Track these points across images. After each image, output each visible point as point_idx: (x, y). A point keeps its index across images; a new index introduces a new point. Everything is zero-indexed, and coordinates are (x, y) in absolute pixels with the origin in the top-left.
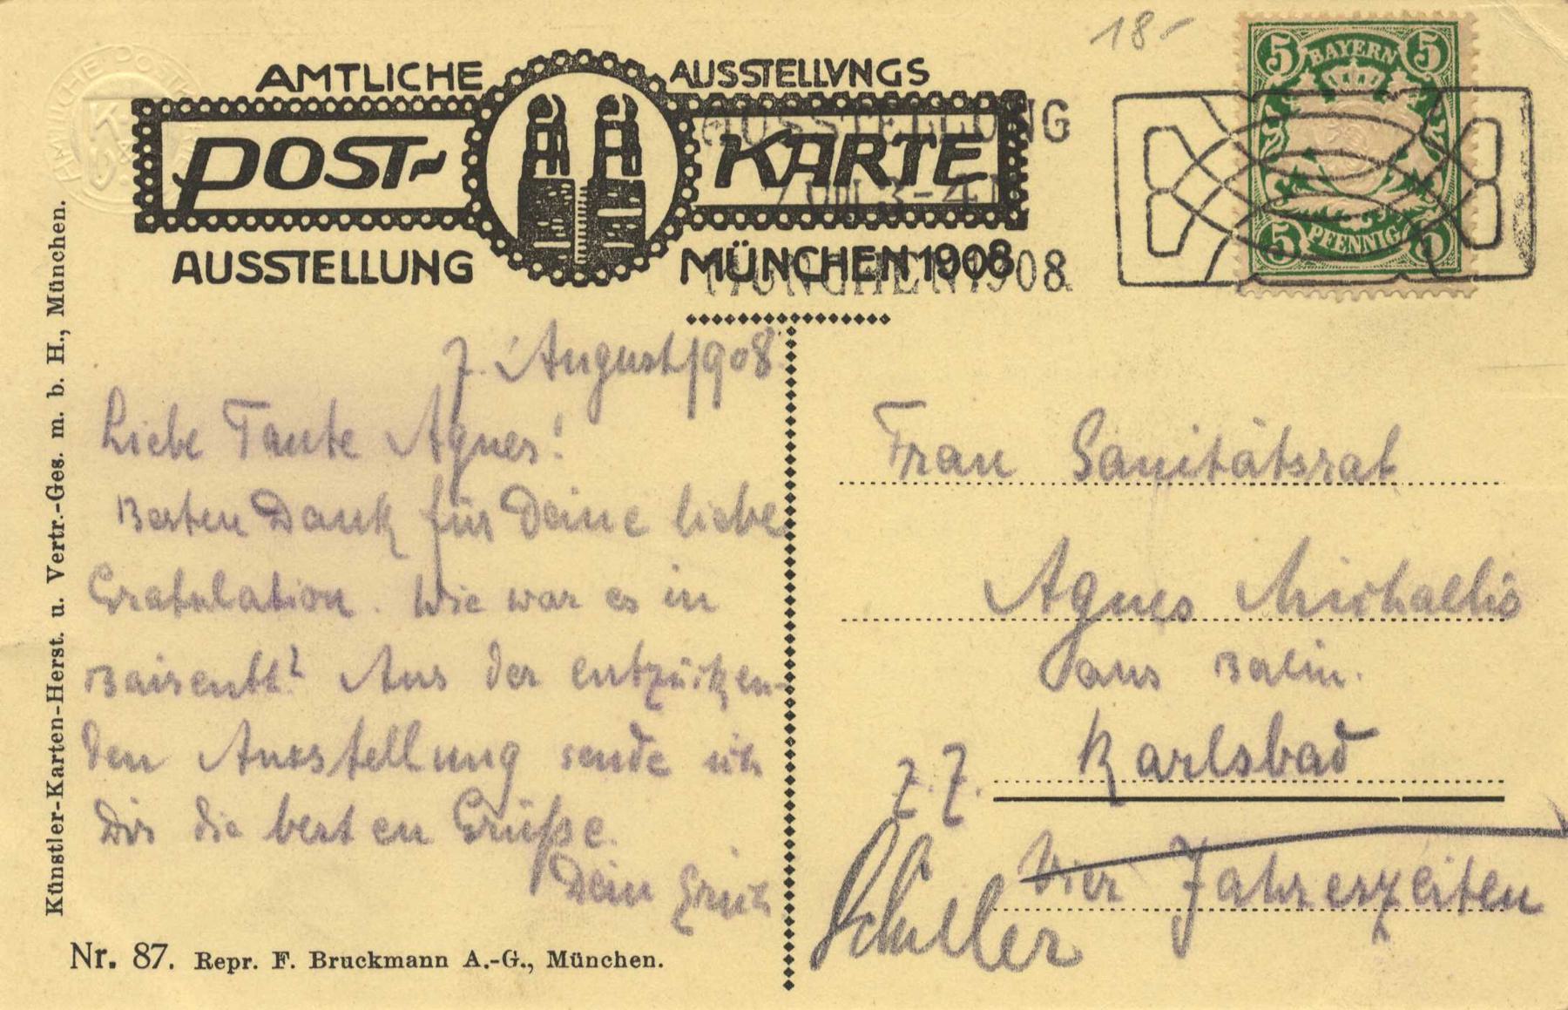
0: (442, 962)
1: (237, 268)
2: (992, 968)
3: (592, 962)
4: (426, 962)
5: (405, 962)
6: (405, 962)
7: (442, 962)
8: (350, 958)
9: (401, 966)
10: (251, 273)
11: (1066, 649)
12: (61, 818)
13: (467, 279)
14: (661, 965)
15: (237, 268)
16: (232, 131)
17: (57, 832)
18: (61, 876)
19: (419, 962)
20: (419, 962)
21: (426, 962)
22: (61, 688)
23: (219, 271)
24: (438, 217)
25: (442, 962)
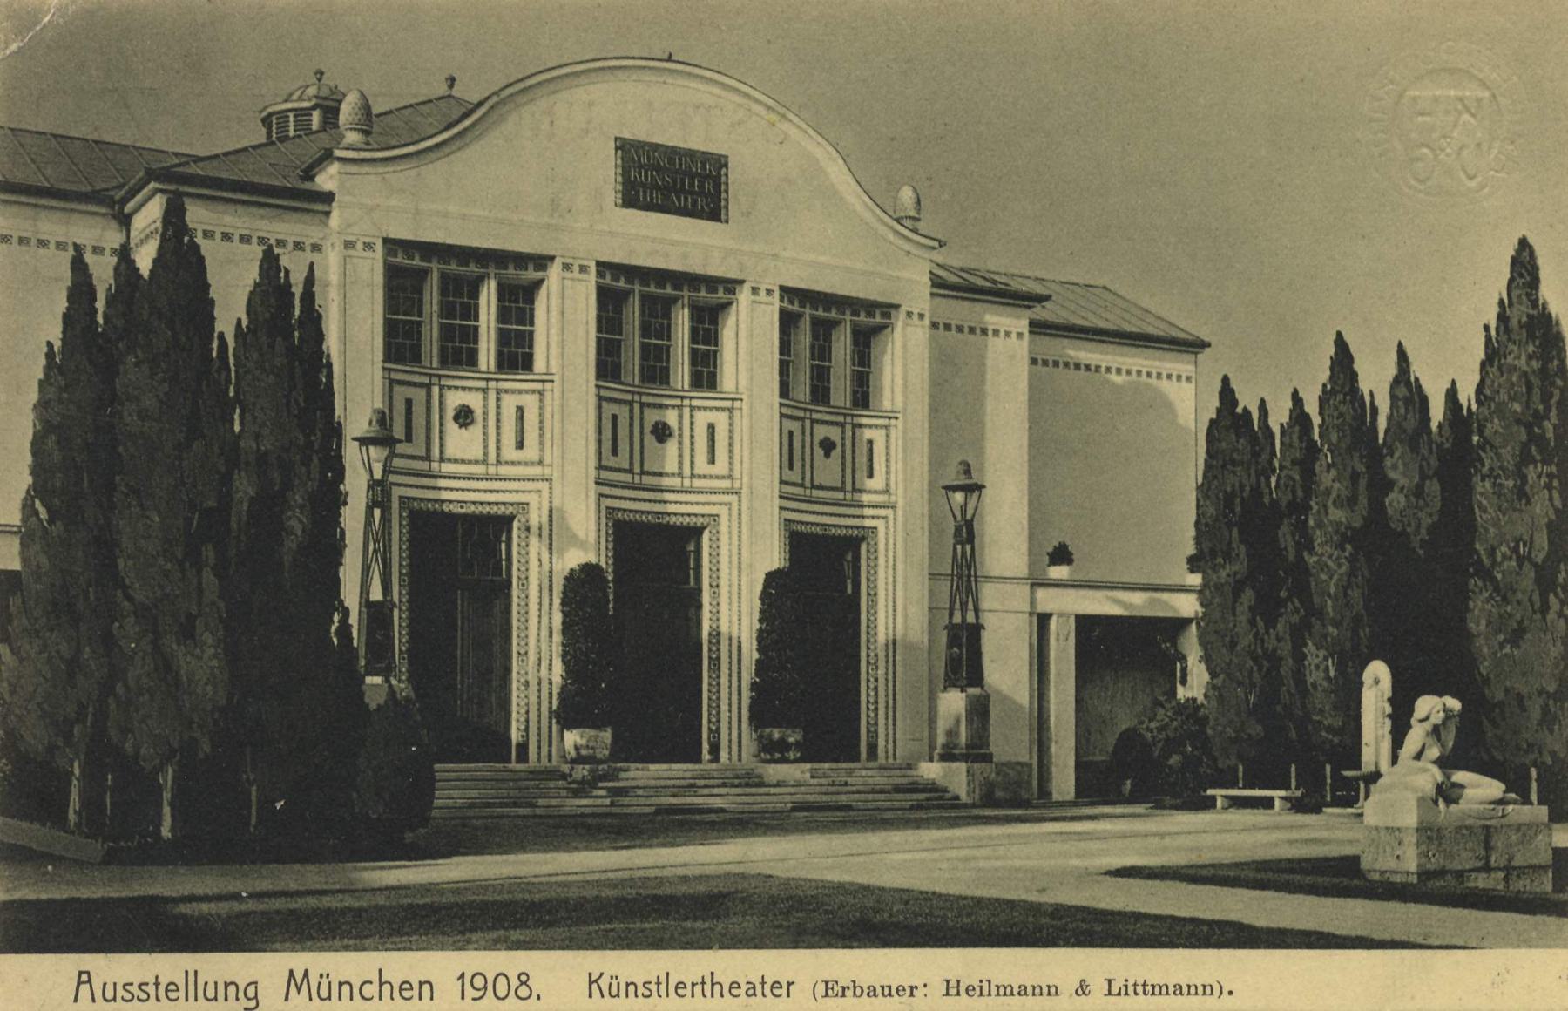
0: (1053, 991)
1: (121, 992)
2: (232, 983)
3: (1193, 990)
4: (1037, 991)
5: (1171, 990)
6: (1171, 990)
7: (1053, 990)
8: (890, 987)
9: (1167, 994)
10: (128, 996)
11: (292, 982)
12: (912, 995)
13: (81, 973)
14: (1230, 993)
15: (121, 992)
16: (1414, 910)
17: (967, 991)
18: (1204, 994)
19: (1185, 990)
20: (1185, 990)
21: (1037, 991)
22: (958, 994)
23: (109, 995)
24: (681, 417)
25: (1053, 991)
